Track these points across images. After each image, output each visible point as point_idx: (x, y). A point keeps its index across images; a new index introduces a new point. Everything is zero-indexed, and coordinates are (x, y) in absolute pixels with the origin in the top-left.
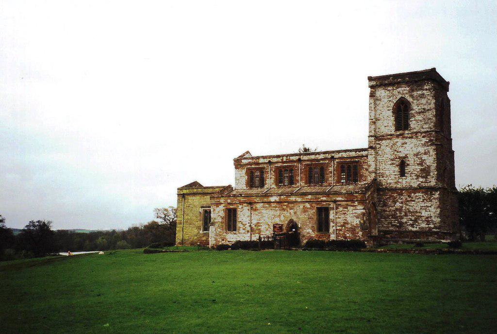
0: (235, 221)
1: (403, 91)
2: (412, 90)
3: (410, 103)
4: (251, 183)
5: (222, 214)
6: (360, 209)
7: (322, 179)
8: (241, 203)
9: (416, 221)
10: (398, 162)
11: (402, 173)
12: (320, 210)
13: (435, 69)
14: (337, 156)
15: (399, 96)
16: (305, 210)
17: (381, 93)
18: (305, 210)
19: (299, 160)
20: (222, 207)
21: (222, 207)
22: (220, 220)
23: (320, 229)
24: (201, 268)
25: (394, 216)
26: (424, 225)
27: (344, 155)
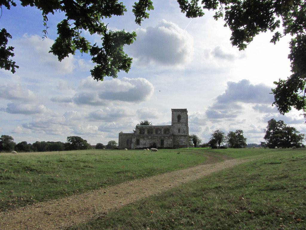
0: (139, 143)
1: (179, 113)
2: (181, 113)
3: (107, 122)
4: (140, 133)
5: (135, 140)
6: (171, 140)
7: (152, 133)
8: (141, 138)
9: (182, 143)
10: (178, 129)
11: (179, 132)
12: (161, 140)
13: (186, 109)
14: (156, 127)
15: (179, 114)
16: (158, 140)
17: (175, 113)
18: (158, 140)
19: (146, 128)
20: (135, 139)
21: (135, 139)
22: (135, 142)
23: (161, 145)
24: (260, 186)
25: (177, 142)
26: (184, 144)
27: (158, 127)
